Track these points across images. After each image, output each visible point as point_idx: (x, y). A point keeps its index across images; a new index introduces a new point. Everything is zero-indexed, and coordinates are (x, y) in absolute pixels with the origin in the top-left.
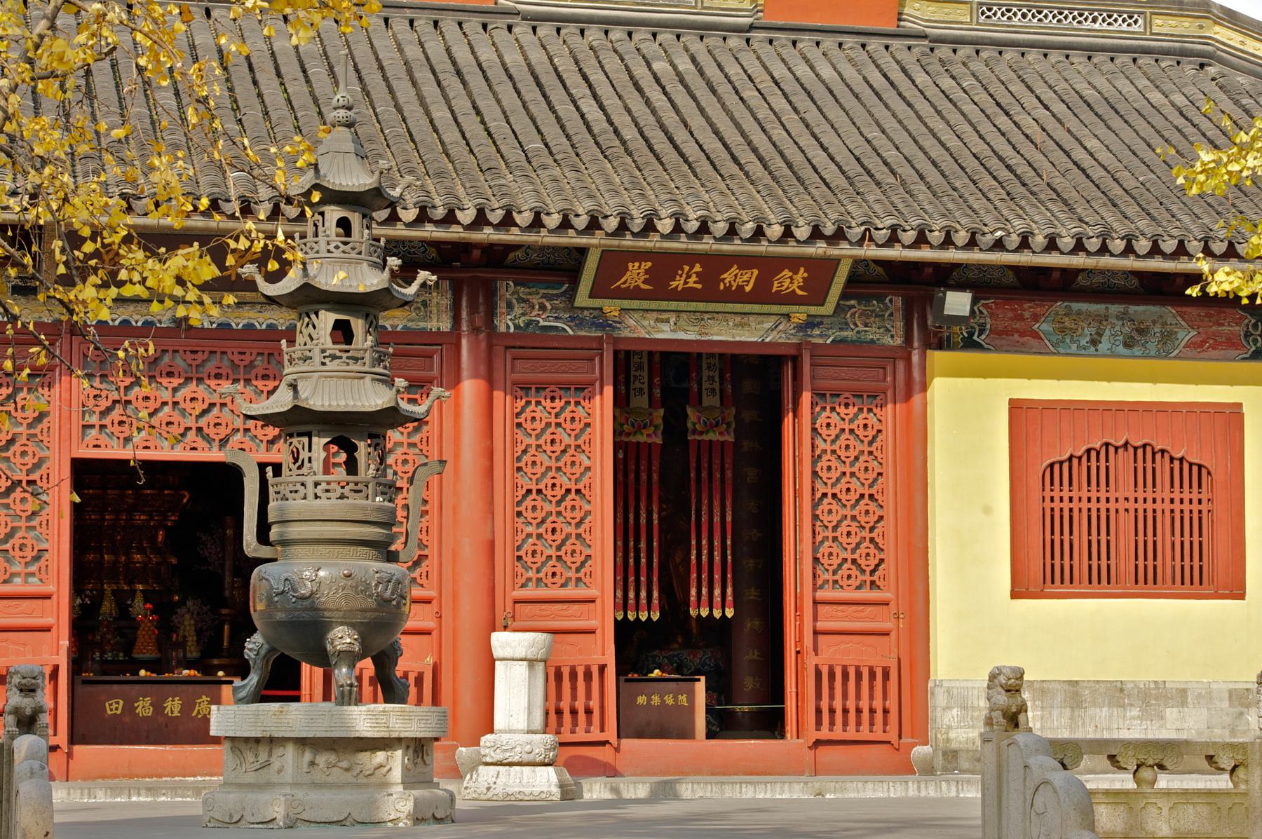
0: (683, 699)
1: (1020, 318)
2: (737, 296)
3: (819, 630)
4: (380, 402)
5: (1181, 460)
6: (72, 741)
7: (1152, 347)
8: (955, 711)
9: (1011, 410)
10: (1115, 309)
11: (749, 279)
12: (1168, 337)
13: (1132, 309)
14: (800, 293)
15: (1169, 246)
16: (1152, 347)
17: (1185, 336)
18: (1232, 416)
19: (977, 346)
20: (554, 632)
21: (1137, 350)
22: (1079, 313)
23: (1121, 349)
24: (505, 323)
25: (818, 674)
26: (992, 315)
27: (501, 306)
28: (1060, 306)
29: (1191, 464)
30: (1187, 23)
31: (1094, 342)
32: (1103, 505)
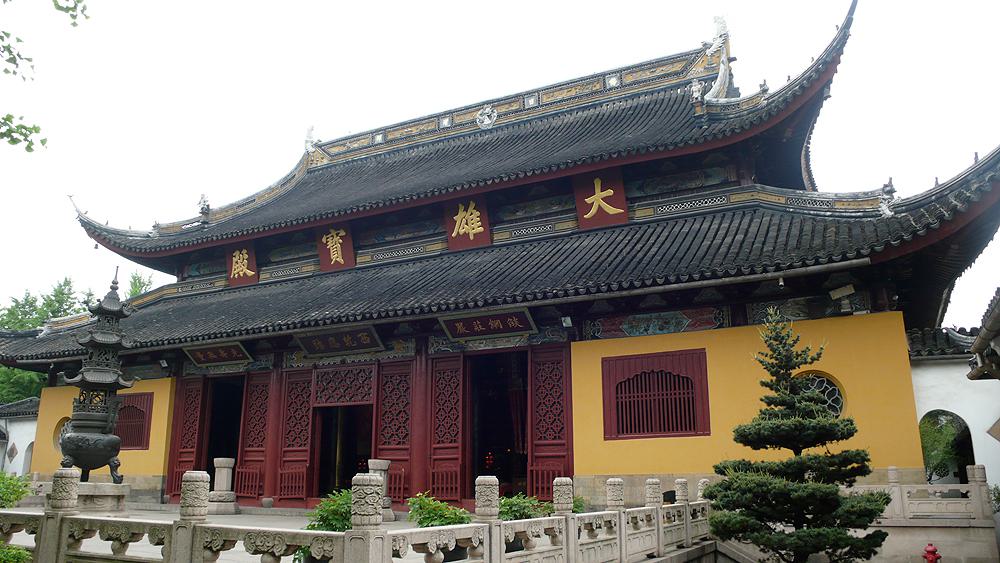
0: (524, 484)
1: (613, 324)
2: (497, 331)
3: (537, 448)
4: (110, 379)
5: (678, 376)
6: (307, 497)
7: (672, 328)
8: (581, 489)
9: (602, 363)
10: (654, 315)
11: (497, 323)
12: (679, 324)
13: (662, 314)
14: (611, 210)
15: (625, 285)
16: (672, 328)
17: (686, 322)
18: (698, 357)
19: (597, 338)
20: (391, 460)
21: (665, 331)
22: (639, 319)
23: (658, 331)
24: (431, 351)
25: (433, 475)
26: (603, 325)
27: (430, 345)
28: (631, 317)
29: (683, 378)
30: (746, 195)
31: (646, 330)
32: (636, 399)
